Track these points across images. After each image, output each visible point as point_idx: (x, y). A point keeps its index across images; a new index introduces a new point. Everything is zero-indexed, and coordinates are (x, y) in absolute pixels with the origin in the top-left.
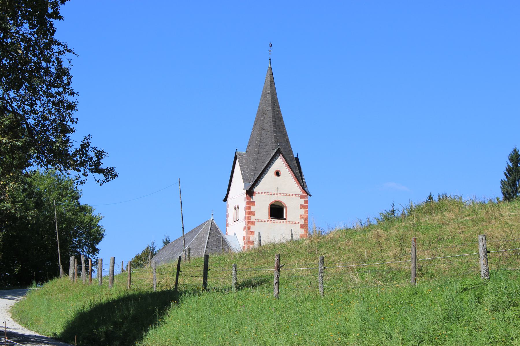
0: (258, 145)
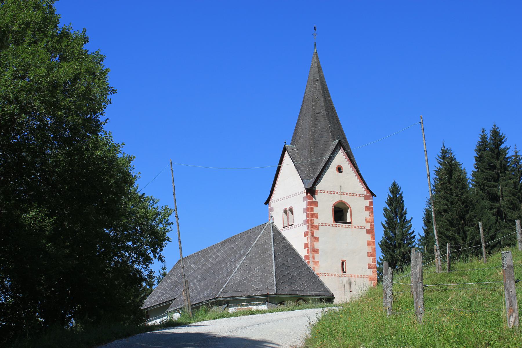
0: (313, 137)
